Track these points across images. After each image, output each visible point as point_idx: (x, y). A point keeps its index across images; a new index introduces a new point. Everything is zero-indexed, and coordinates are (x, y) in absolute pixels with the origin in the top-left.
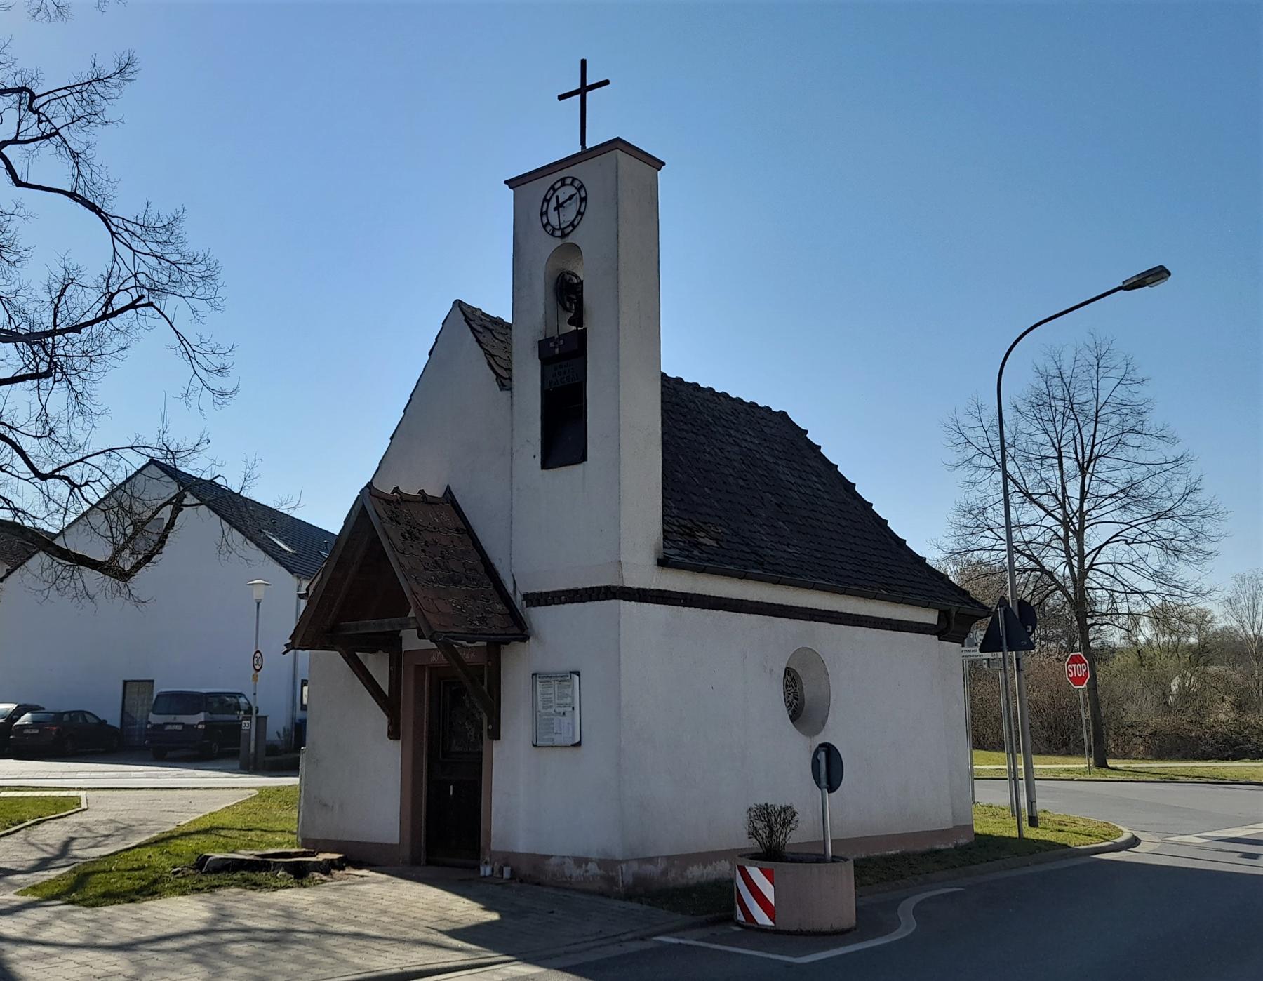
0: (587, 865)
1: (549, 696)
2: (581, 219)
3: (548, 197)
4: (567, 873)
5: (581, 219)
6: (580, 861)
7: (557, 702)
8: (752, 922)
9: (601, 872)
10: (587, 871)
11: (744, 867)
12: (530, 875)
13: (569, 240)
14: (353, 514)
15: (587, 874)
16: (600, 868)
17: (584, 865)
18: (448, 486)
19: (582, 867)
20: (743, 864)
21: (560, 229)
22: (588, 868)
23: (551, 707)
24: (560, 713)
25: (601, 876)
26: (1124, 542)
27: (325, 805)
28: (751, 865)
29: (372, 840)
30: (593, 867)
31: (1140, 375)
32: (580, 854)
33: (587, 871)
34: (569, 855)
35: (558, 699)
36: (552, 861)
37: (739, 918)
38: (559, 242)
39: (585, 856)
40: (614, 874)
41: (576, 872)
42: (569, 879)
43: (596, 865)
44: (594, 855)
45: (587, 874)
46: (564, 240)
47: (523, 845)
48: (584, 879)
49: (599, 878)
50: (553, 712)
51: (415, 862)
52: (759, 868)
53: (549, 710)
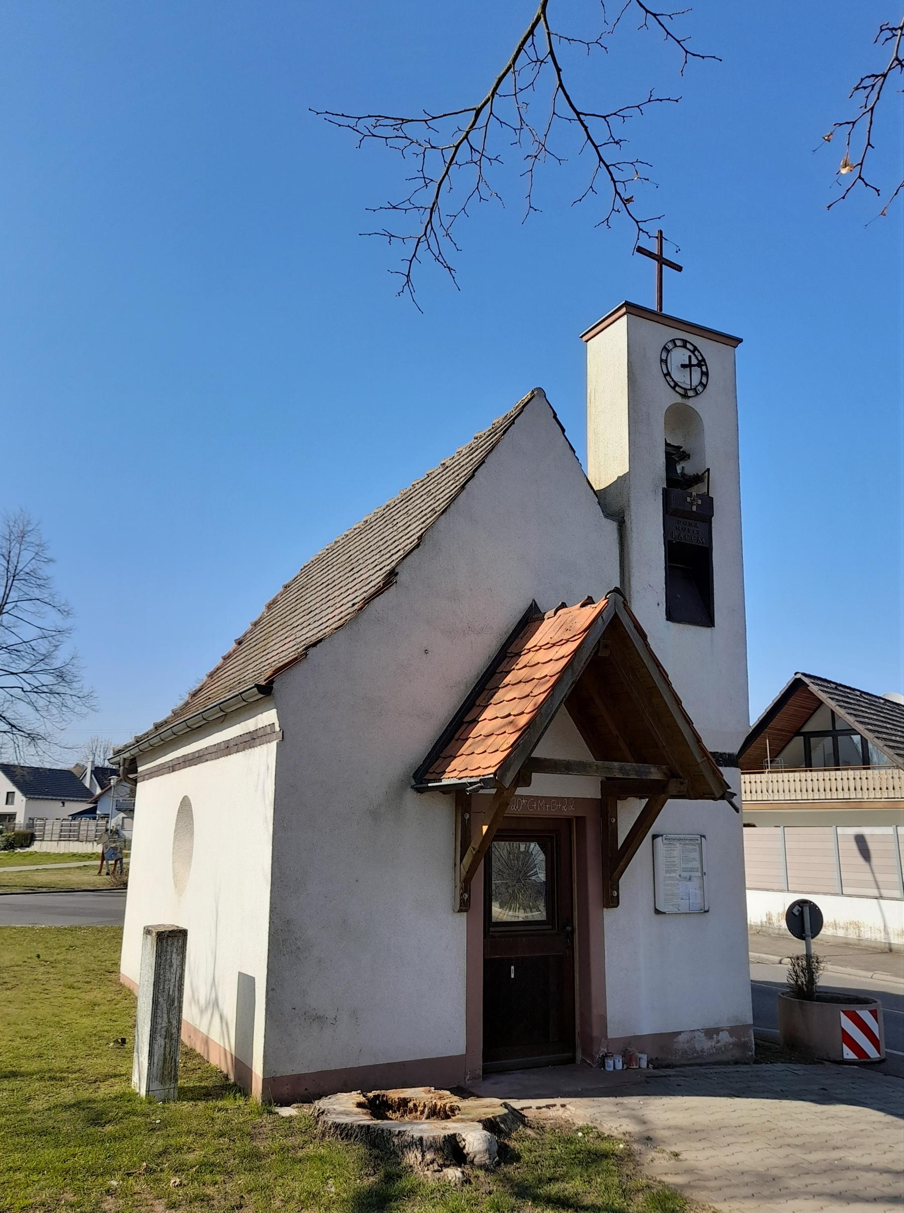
0: (718, 1034)
1: (672, 859)
2: (669, 384)
3: (696, 353)
4: (698, 1047)
5: (669, 384)
6: (710, 1033)
7: (683, 866)
8: (867, 1058)
9: (732, 1040)
10: (718, 1042)
11: (855, 1012)
12: (657, 1059)
13: (690, 402)
14: (600, 620)
15: (719, 1044)
16: (731, 1036)
17: (715, 1036)
18: (534, 600)
19: (713, 1038)
20: (854, 1010)
21: (691, 389)
22: (719, 1038)
23: (674, 871)
24: (685, 878)
25: (734, 1044)
26: (21, 689)
27: (319, 1018)
28: (861, 1009)
29: (382, 1061)
30: (725, 1037)
31: (48, 554)
32: (711, 1025)
33: (718, 1042)
34: (700, 1028)
35: (683, 864)
36: (681, 1038)
37: (846, 1057)
38: (679, 399)
39: (717, 1026)
40: (747, 1039)
41: (706, 1045)
42: (701, 1053)
43: (727, 1033)
44: (724, 1024)
45: (719, 1044)
46: (684, 400)
47: (647, 1026)
48: (716, 1050)
49: (731, 1046)
50: (678, 877)
51: (487, 1072)
52: (869, 1011)
53: (673, 875)
